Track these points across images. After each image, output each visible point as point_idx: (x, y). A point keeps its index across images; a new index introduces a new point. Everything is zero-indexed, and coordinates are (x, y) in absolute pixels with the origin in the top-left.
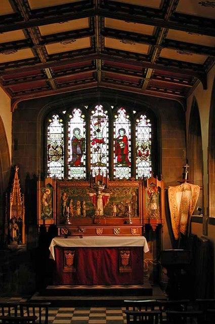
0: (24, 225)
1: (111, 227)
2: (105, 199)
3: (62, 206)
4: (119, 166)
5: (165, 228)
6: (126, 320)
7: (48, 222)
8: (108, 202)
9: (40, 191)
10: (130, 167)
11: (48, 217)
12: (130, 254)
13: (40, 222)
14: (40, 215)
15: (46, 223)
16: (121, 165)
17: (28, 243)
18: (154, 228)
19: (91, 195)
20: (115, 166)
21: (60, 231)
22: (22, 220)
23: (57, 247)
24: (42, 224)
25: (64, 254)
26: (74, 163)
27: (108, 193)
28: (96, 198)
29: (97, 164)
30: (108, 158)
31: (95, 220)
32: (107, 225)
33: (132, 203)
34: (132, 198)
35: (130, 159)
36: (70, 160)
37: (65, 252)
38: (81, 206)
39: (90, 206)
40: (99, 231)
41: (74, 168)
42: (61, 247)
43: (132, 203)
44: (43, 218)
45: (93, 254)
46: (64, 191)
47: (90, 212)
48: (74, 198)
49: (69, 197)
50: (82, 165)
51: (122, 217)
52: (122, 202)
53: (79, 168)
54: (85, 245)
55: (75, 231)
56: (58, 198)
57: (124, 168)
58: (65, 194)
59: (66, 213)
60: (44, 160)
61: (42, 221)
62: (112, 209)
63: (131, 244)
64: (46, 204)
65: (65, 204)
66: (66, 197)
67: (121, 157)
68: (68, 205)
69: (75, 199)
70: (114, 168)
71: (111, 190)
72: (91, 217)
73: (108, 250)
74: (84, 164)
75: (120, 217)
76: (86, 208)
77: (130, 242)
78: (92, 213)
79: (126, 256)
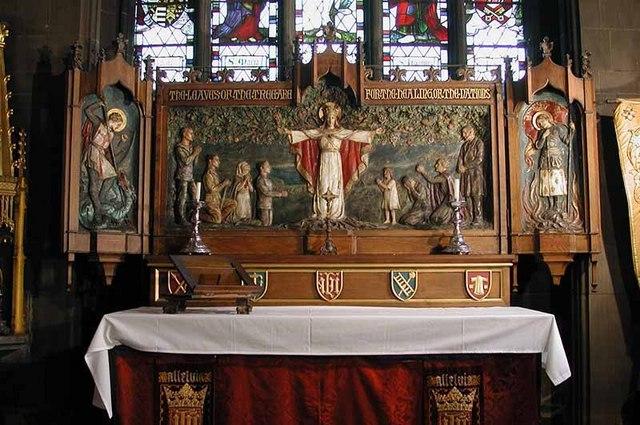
0: (20, 258)
1: (379, 268)
2: (350, 153)
3: (179, 183)
4: (402, 41)
5: (601, 273)
6: (362, 32)
7: (112, 244)
8: (363, 168)
9: (77, 112)
10: (443, 47)
11: (114, 221)
12: (480, 389)
13: (76, 243)
14: (73, 215)
15: (101, 247)
16: (410, 39)
17: (35, 330)
18: (558, 271)
19: (297, 137)
20: (386, 40)
21: (163, 281)
22: (13, 235)
23: (122, 353)
24: (87, 249)
25: (157, 387)
26: (234, 31)
27: (367, 128)
28: (317, 149)
29: (320, 34)
30: (361, 13)
31: (312, 239)
32: (360, 259)
33: (463, 169)
34: (463, 153)
35: (444, 19)
36: (217, 19)
37: (163, 377)
38: (255, 183)
39: (289, 182)
40: (327, 283)
41: (235, 49)
42: (134, 350)
43: (463, 169)
44: (90, 228)
45: (299, 386)
46: (188, 119)
47: (291, 207)
48: (225, 151)
49: (206, 147)
50: (262, 38)
51: (422, 228)
52: (421, 169)
53: (252, 49)
54: (195, 349)
55: (217, 280)
56: (160, 148)
57: (424, 49)
58: (190, 135)
59: (191, 205)
60: (120, 16)
61: (86, 238)
62: (383, 194)
63: (467, 345)
64: (107, 169)
65: (188, 174)
66: (193, 144)
67: (409, 9)
68: (201, 175)
69: (230, 153)
70: (386, 49)
71: (376, 119)
72: (294, 229)
73: (373, 374)
74: (273, 33)
75: (416, 227)
76: (274, 190)
77: (483, 334)
78: (296, 213)
79: (459, 400)
